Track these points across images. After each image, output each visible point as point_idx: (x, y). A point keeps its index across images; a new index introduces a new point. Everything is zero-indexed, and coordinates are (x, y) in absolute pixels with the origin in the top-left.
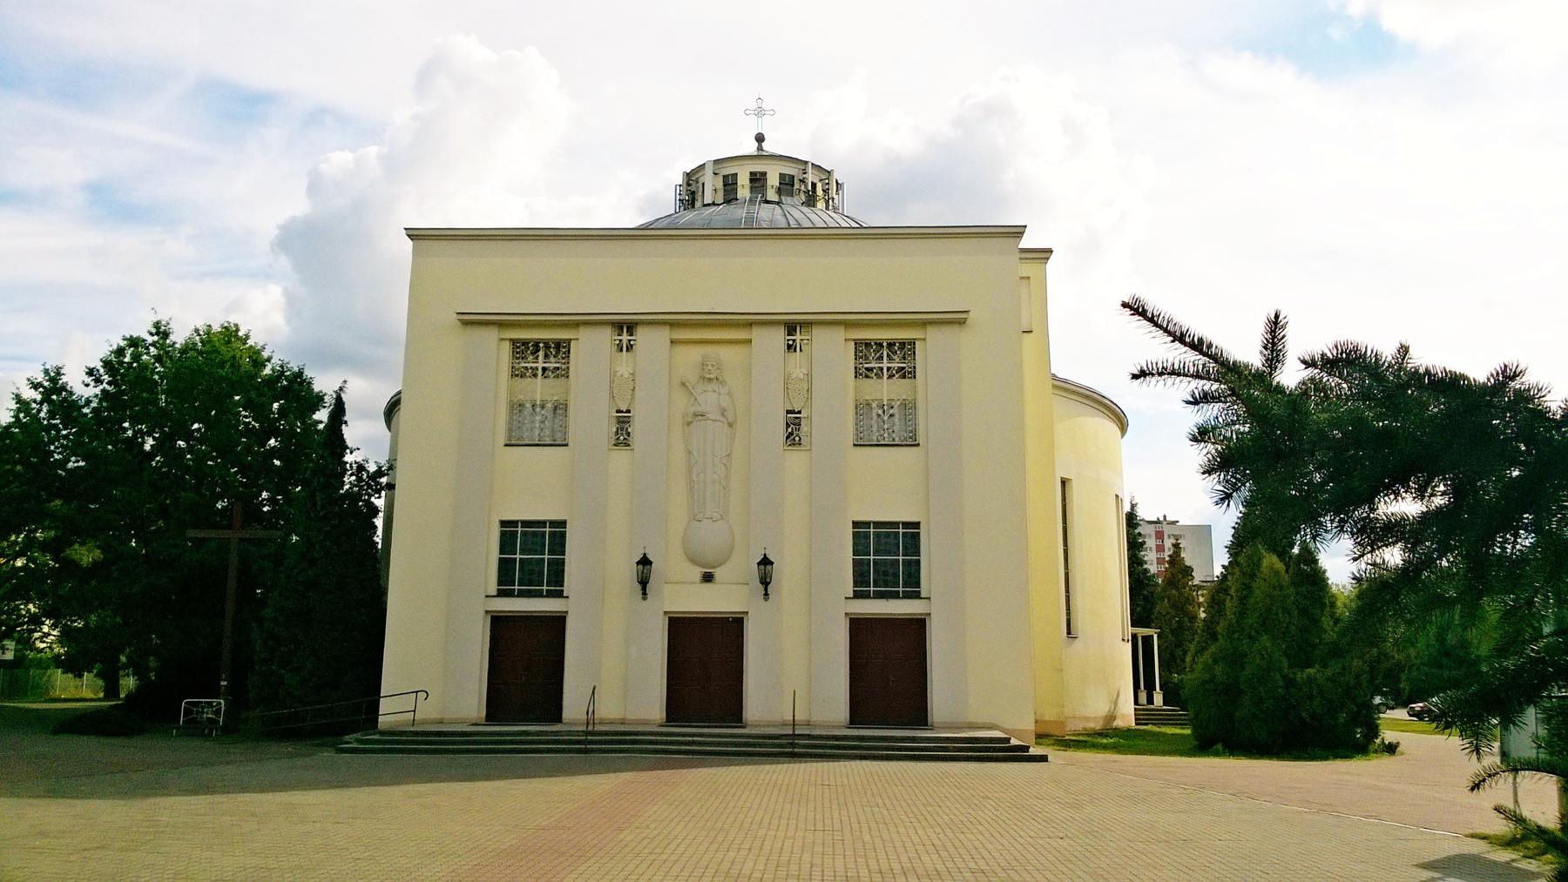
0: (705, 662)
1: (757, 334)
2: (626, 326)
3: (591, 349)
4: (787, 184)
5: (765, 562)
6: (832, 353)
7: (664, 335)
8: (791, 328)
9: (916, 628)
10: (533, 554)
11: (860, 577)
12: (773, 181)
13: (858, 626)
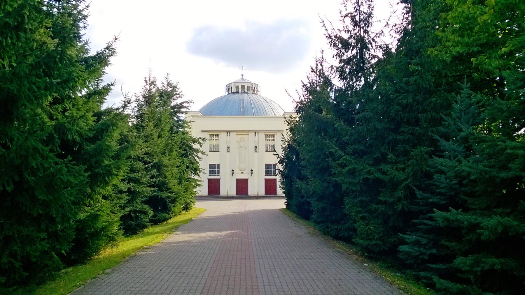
0: (242, 187)
1: (250, 133)
2: (228, 132)
3: (223, 136)
4: (249, 88)
5: (252, 170)
6: (262, 136)
7: (235, 133)
8: (255, 133)
9: (219, 180)
10: (214, 169)
11: (266, 172)
12: (246, 87)
13: (266, 180)
